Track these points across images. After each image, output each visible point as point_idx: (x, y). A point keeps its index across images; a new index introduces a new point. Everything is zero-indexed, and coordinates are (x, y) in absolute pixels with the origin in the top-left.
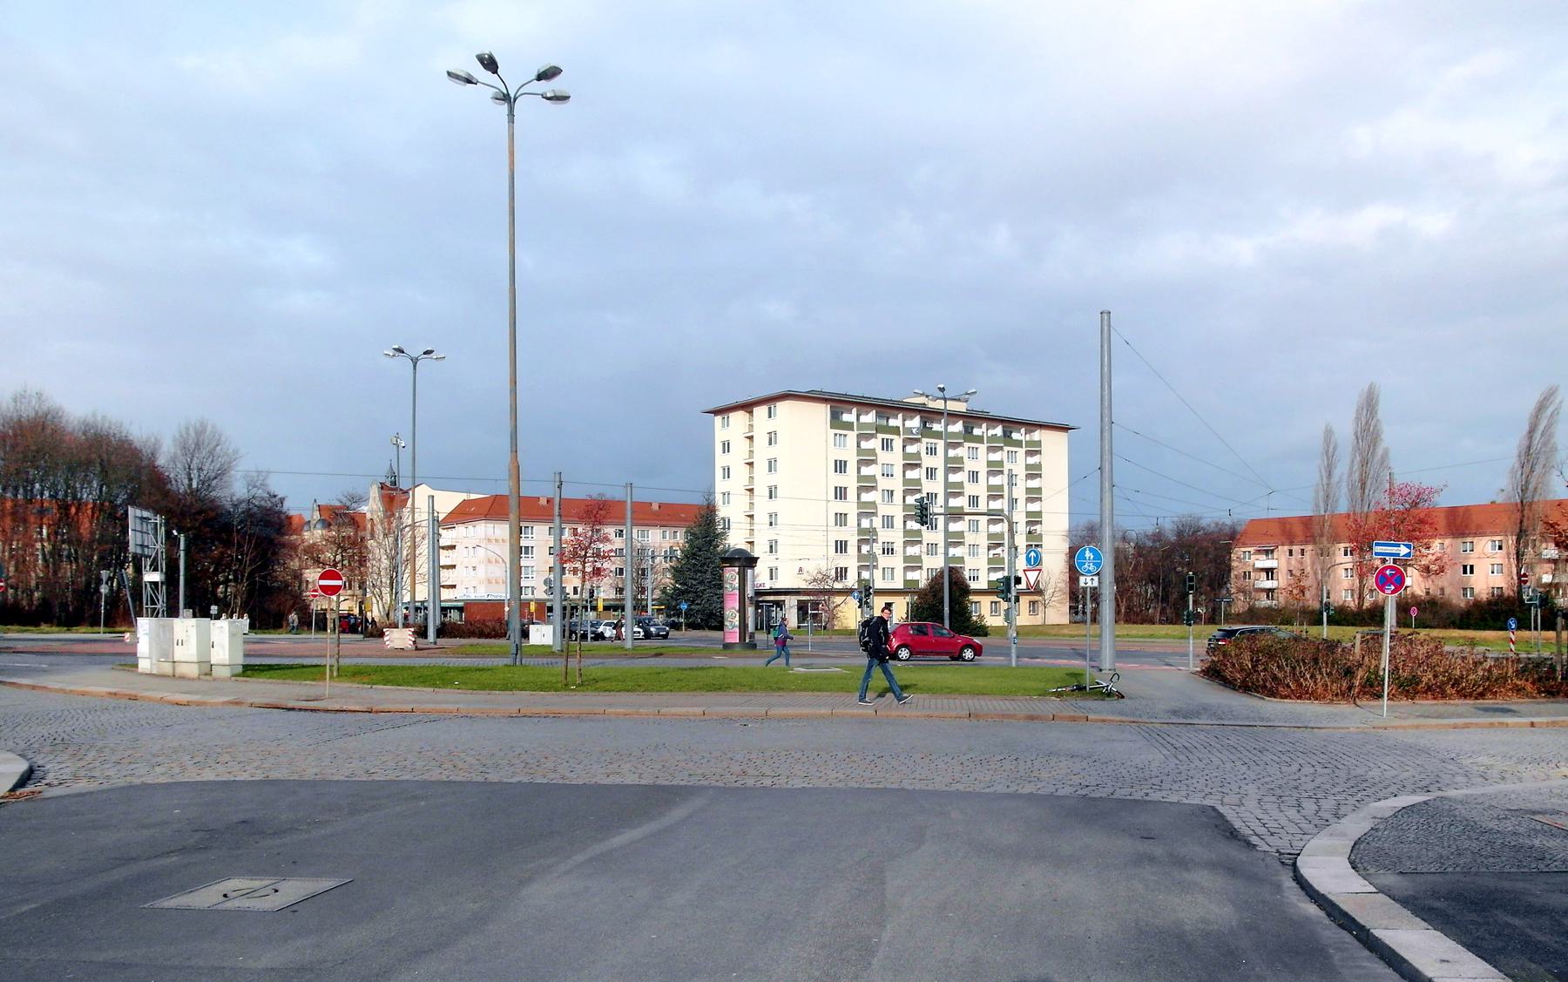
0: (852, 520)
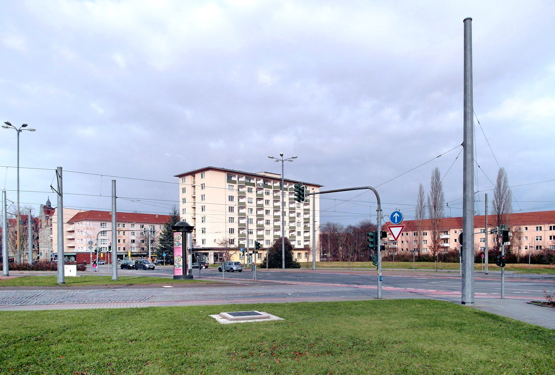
0: (236, 220)
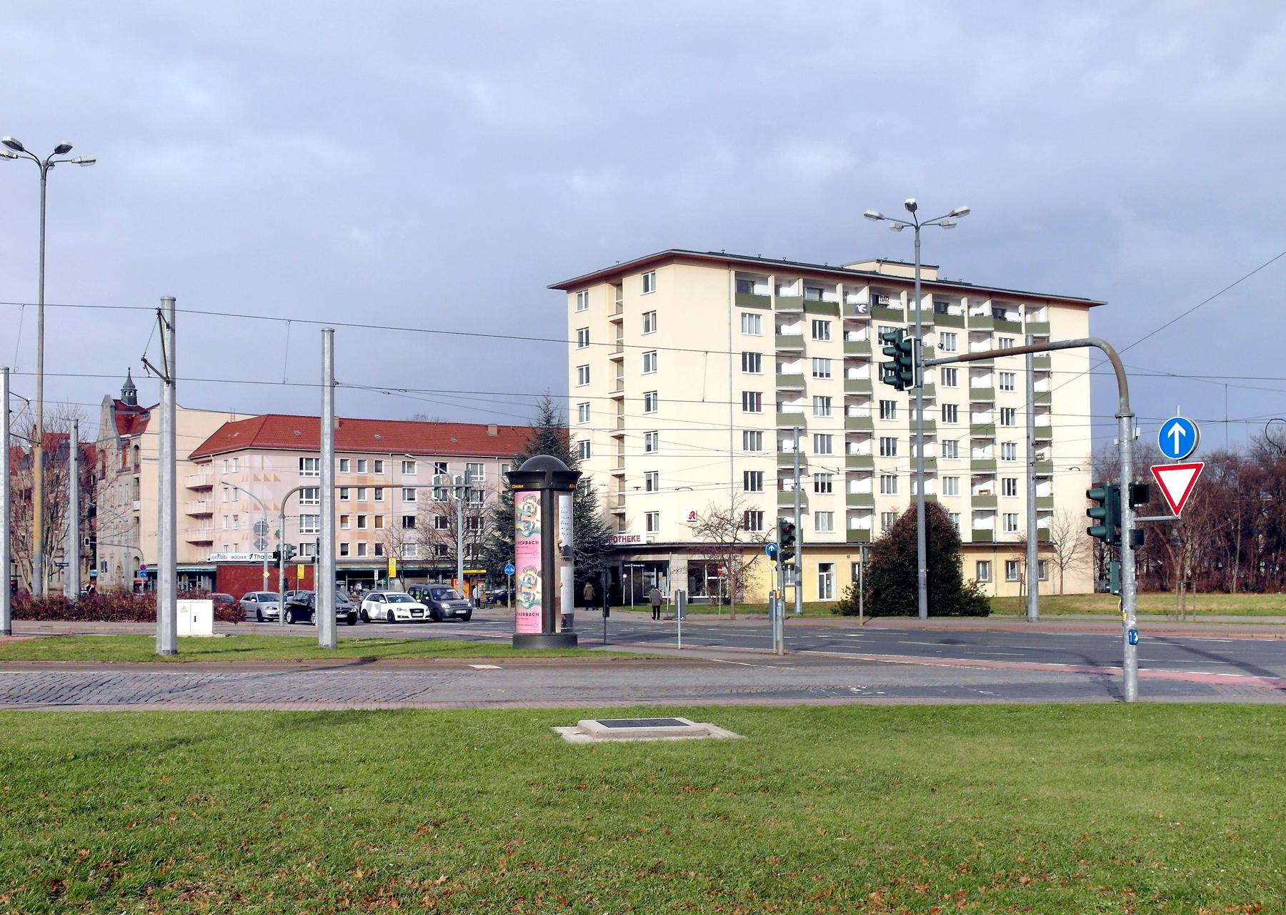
0: (769, 440)
